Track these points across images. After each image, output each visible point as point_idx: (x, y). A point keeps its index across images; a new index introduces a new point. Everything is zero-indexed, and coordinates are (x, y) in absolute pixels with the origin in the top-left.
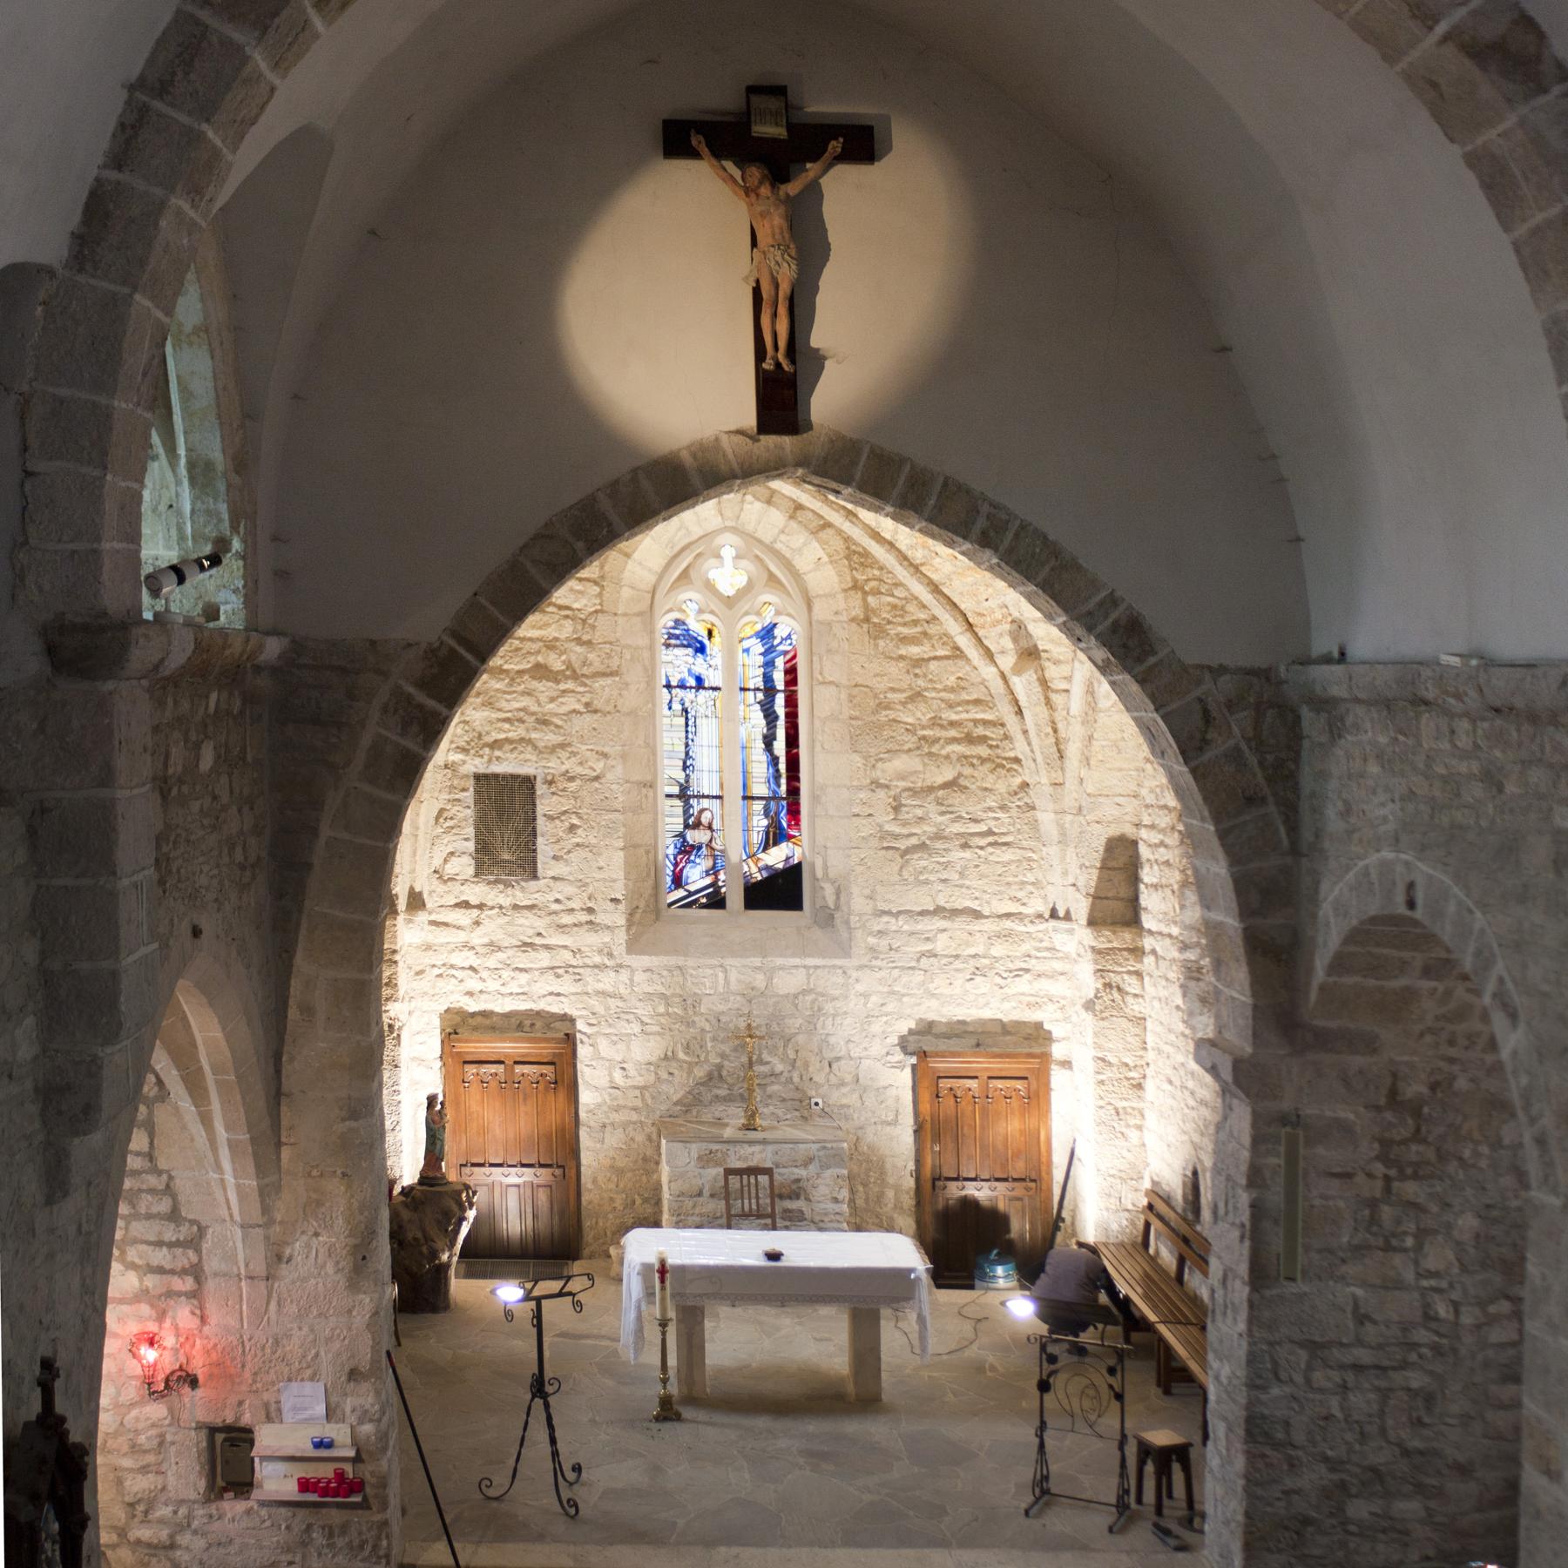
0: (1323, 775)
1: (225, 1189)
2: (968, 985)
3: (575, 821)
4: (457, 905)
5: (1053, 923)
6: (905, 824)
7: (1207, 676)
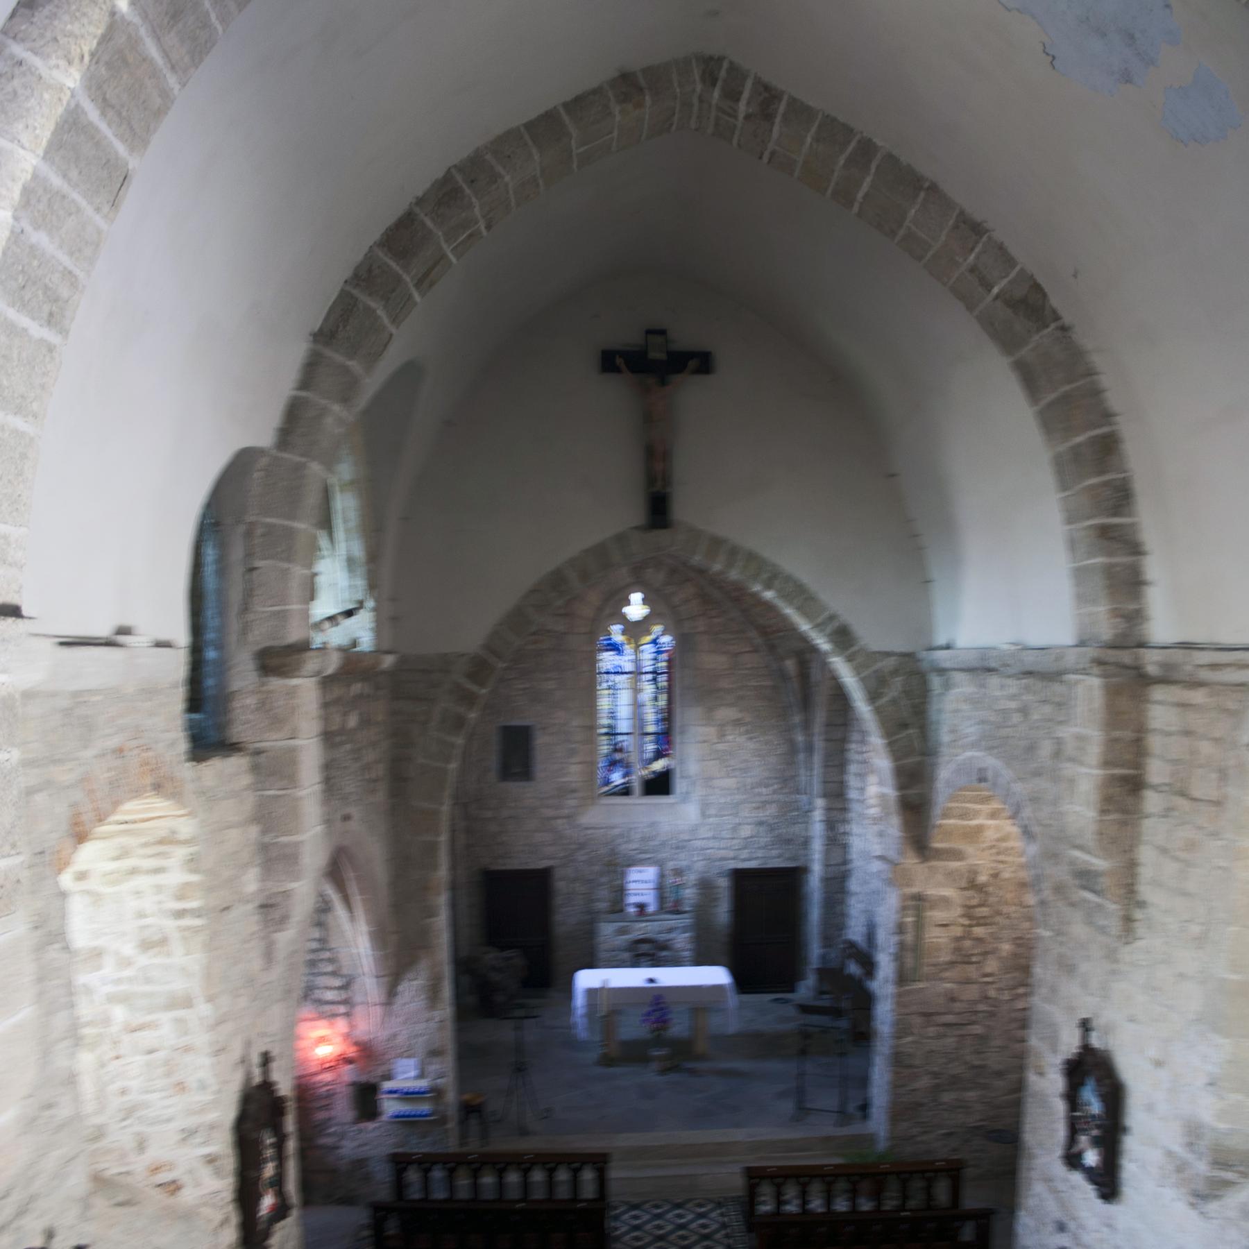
0: (940, 711)
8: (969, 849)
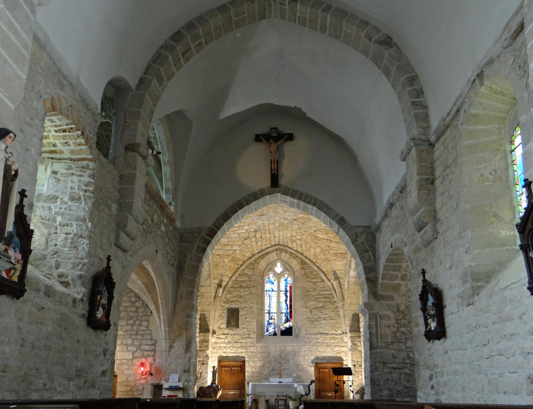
1: (162, 332)
2: (326, 349)
3: (247, 316)
4: (223, 334)
6: (313, 315)
7: (357, 228)
8: (396, 296)
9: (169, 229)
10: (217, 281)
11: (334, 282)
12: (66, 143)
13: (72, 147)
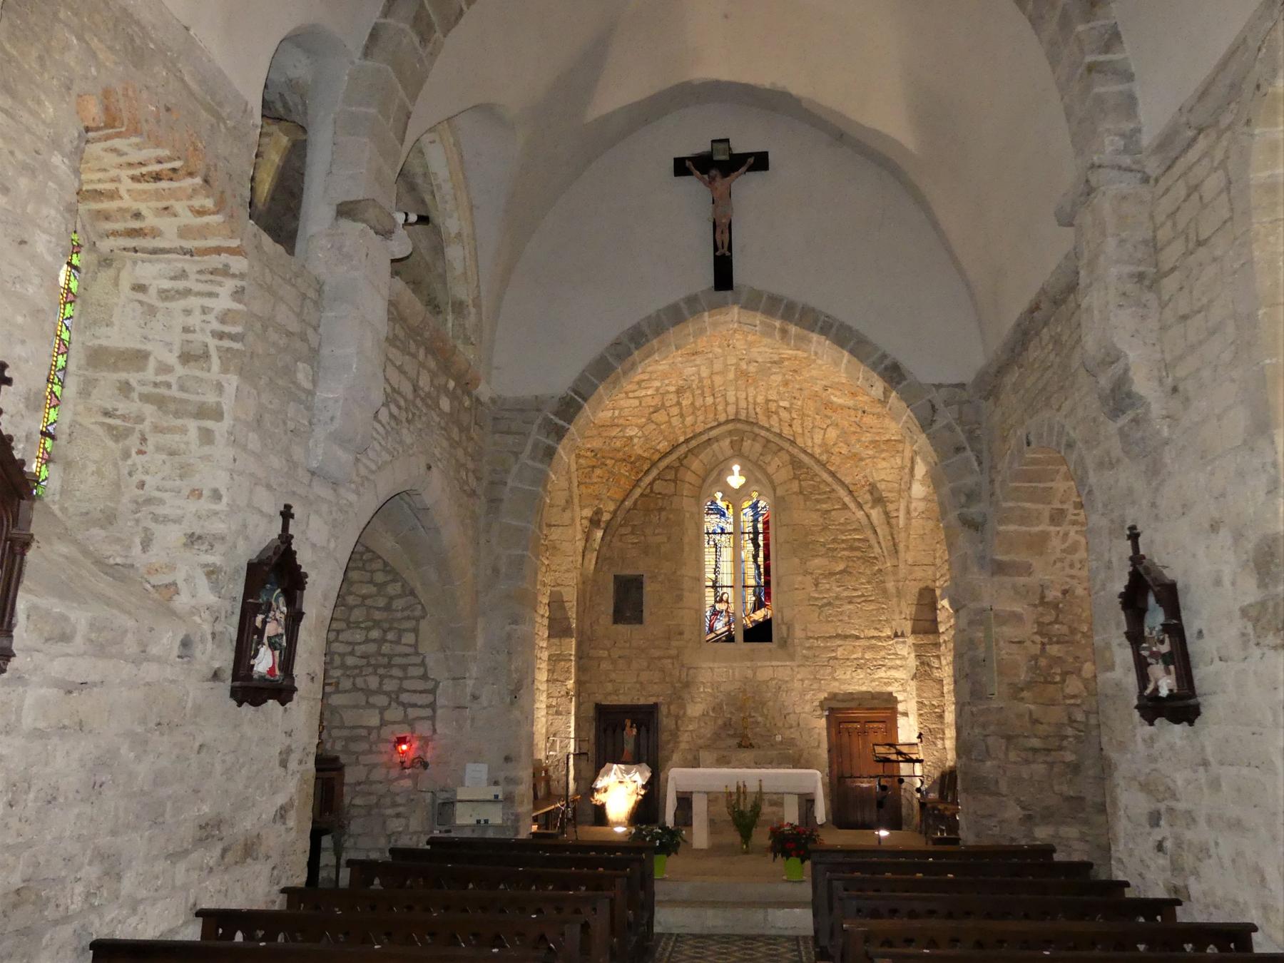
2: (854, 674)
5: (896, 640)
6: (821, 592)
8: (1037, 563)
9: (461, 403)
10: (588, 512)
11: (872, 511)
12: (166, 209)
13: (187, 218)
